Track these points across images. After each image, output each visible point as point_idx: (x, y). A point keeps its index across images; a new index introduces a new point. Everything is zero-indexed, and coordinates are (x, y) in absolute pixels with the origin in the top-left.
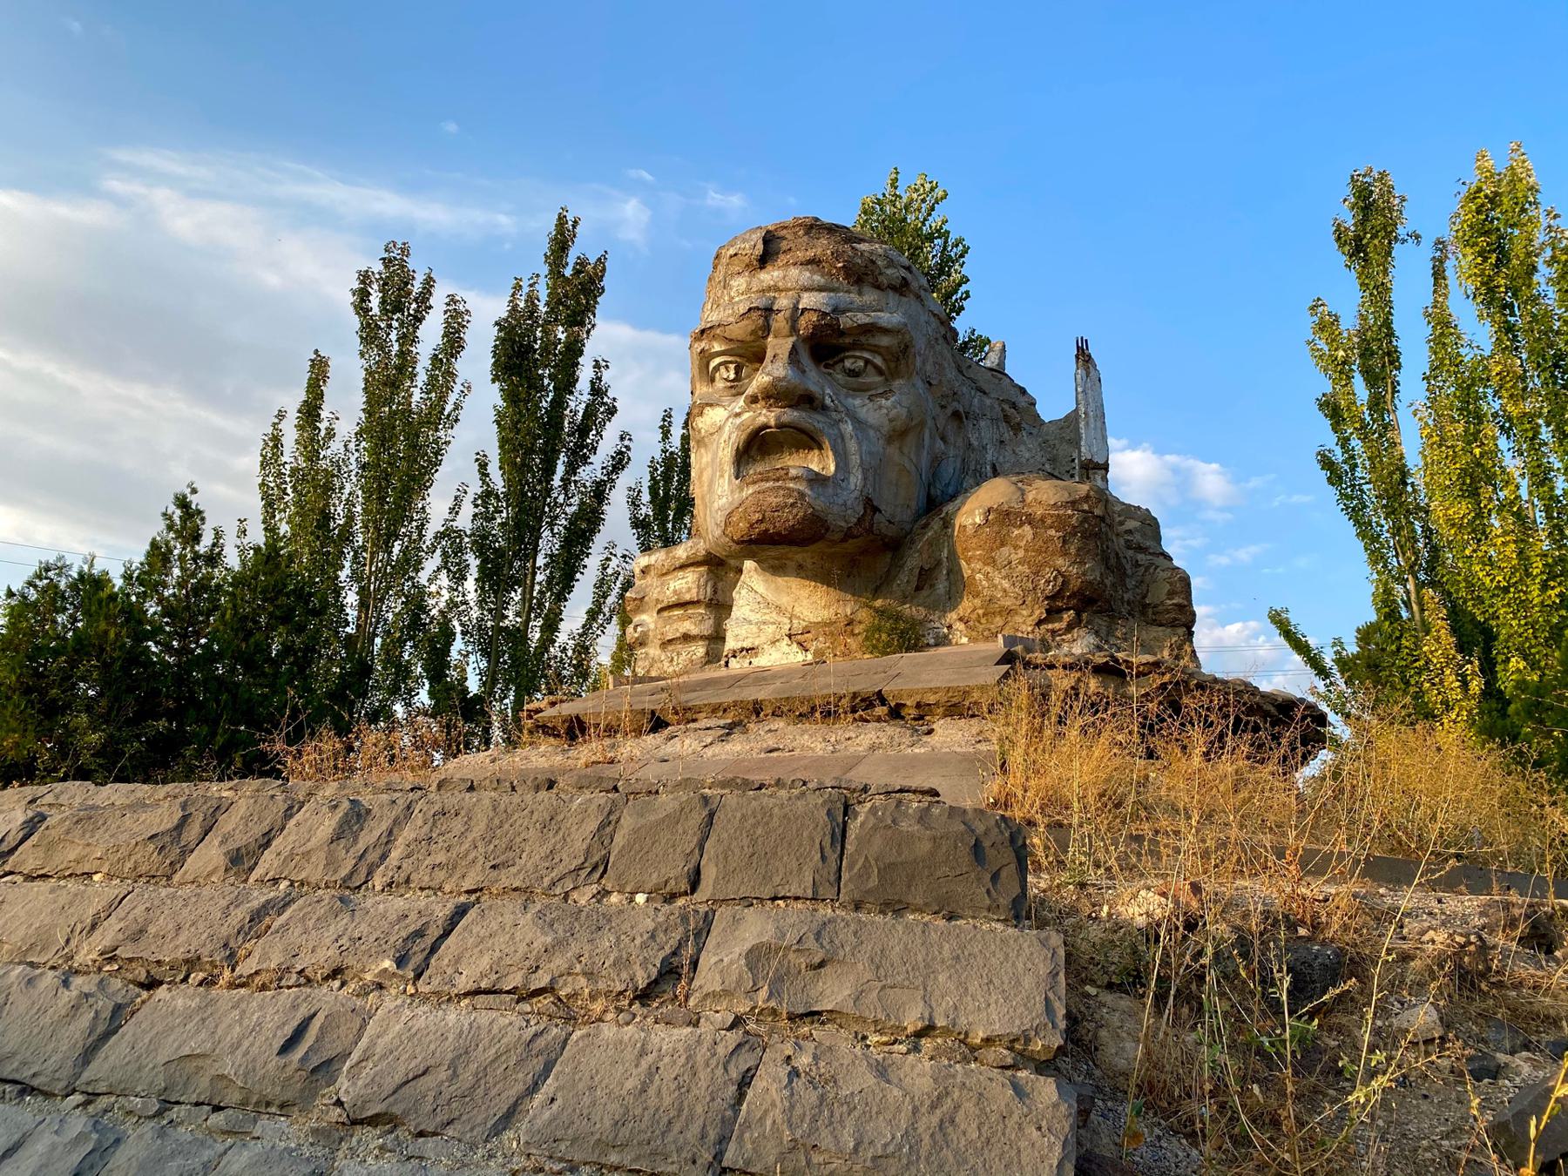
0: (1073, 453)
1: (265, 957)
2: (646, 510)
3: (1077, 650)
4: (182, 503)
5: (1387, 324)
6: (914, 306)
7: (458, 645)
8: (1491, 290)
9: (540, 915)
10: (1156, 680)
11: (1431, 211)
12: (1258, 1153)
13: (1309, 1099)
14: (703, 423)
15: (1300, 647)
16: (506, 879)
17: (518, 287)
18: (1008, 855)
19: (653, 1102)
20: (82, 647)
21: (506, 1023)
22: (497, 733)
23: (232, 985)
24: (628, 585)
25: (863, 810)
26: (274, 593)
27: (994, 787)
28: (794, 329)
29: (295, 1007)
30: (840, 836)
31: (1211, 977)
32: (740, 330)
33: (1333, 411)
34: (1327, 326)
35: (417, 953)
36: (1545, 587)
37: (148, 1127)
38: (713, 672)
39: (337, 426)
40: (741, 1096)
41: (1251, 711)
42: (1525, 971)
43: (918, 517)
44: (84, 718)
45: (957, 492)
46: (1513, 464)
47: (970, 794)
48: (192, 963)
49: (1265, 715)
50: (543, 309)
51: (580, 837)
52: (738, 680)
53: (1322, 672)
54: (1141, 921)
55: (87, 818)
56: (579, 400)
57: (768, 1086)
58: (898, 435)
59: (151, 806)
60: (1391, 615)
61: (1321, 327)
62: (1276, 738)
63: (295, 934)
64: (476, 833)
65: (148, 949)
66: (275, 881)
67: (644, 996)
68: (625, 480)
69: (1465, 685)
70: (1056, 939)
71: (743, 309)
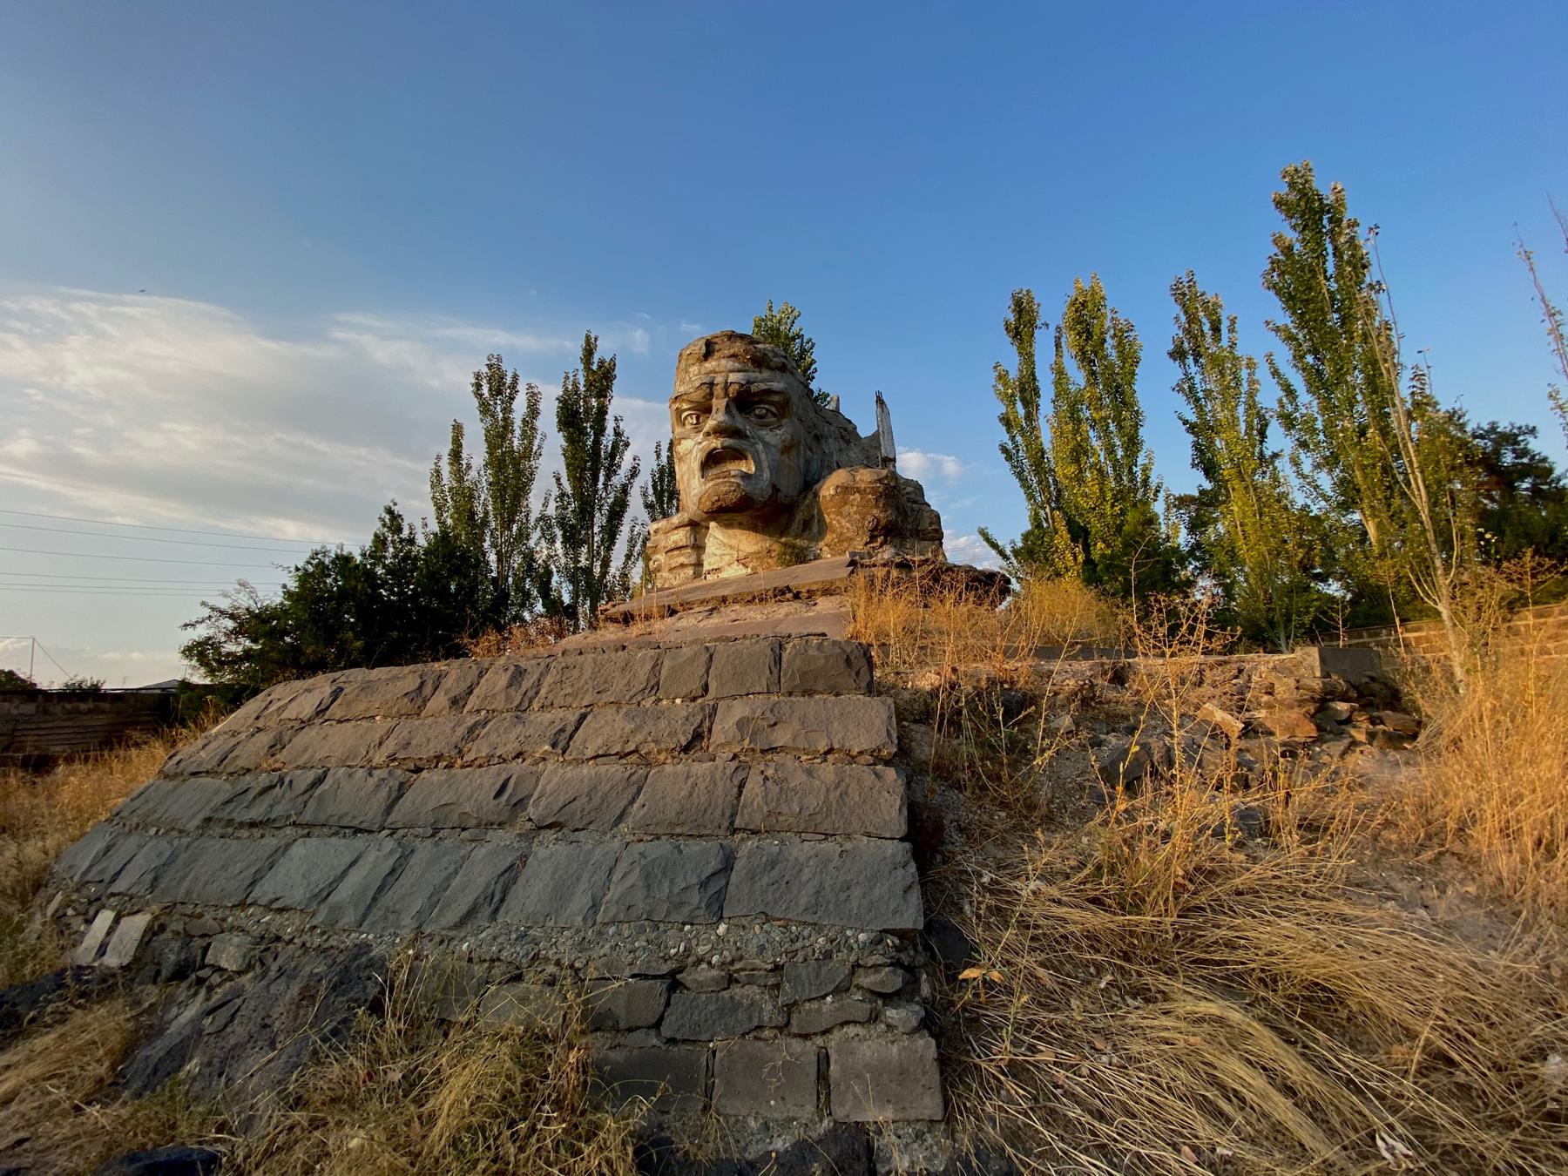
0: (877, 453)
1: (479, 750)
2: (652, 498)
3: (886, 556)
4: (390, 511)
5: (1033, 374)
6: (791, 378)
7: (555, 579)
8: (1084, 353)
9: (626, 714)
10: (926, 568)
11: (1053, 312)
12: (992, 793)
13: (1014, 765)
14: (681, 448)
15: (994, 546)
16: (606, 697)
17: (567, 378)
18: (863, 662)
19: (696, 801)
20: (343, 594)
21: (614, 770)
22: (582, 623)
23: (463, 767)
24: (646, 540)
25: (789, 647)
26: (449, 556)
27: (850, 628)
28: (726, 394)
29: (499, 774)
30: (778, 660)
31: (965, 711)
32: (697, 396)
33: (1007, 422)
34: (1003, 377)
35: (562, 741)
36: (1113, 506)
37: (428, 842)
38: (698, 583)
39: (473, 462)
40: (740, 793)
41: (973, 580)
42: (1111, 695)
43: (801, 492)
44: (350, 634)
45: (820, 478)
46: (1096, 444)
47: (839, 634)
48: (439, 758)
49: (980, 581)
50: (582, 389)
51: (643, 673)
52: (713, 586)
53: (1005, 557)
54: (928, 688)
55: (367, 687)
56: (608, 440)
57: (754, 786)
58: (787, 449)
59: (404, 677)
60: (1038, 526)
61: (1000, 377)
62: (987, 592)
63: (493, 737)
64: (586, 676)
65: (411, 753)
66: (478, 711)
67: (686, 749)
68: (638, 482)
69: (1075, 558)
70: (890, 701)
71: (697, 384)
